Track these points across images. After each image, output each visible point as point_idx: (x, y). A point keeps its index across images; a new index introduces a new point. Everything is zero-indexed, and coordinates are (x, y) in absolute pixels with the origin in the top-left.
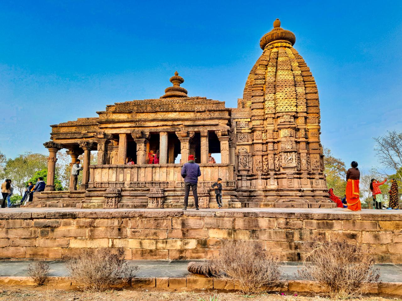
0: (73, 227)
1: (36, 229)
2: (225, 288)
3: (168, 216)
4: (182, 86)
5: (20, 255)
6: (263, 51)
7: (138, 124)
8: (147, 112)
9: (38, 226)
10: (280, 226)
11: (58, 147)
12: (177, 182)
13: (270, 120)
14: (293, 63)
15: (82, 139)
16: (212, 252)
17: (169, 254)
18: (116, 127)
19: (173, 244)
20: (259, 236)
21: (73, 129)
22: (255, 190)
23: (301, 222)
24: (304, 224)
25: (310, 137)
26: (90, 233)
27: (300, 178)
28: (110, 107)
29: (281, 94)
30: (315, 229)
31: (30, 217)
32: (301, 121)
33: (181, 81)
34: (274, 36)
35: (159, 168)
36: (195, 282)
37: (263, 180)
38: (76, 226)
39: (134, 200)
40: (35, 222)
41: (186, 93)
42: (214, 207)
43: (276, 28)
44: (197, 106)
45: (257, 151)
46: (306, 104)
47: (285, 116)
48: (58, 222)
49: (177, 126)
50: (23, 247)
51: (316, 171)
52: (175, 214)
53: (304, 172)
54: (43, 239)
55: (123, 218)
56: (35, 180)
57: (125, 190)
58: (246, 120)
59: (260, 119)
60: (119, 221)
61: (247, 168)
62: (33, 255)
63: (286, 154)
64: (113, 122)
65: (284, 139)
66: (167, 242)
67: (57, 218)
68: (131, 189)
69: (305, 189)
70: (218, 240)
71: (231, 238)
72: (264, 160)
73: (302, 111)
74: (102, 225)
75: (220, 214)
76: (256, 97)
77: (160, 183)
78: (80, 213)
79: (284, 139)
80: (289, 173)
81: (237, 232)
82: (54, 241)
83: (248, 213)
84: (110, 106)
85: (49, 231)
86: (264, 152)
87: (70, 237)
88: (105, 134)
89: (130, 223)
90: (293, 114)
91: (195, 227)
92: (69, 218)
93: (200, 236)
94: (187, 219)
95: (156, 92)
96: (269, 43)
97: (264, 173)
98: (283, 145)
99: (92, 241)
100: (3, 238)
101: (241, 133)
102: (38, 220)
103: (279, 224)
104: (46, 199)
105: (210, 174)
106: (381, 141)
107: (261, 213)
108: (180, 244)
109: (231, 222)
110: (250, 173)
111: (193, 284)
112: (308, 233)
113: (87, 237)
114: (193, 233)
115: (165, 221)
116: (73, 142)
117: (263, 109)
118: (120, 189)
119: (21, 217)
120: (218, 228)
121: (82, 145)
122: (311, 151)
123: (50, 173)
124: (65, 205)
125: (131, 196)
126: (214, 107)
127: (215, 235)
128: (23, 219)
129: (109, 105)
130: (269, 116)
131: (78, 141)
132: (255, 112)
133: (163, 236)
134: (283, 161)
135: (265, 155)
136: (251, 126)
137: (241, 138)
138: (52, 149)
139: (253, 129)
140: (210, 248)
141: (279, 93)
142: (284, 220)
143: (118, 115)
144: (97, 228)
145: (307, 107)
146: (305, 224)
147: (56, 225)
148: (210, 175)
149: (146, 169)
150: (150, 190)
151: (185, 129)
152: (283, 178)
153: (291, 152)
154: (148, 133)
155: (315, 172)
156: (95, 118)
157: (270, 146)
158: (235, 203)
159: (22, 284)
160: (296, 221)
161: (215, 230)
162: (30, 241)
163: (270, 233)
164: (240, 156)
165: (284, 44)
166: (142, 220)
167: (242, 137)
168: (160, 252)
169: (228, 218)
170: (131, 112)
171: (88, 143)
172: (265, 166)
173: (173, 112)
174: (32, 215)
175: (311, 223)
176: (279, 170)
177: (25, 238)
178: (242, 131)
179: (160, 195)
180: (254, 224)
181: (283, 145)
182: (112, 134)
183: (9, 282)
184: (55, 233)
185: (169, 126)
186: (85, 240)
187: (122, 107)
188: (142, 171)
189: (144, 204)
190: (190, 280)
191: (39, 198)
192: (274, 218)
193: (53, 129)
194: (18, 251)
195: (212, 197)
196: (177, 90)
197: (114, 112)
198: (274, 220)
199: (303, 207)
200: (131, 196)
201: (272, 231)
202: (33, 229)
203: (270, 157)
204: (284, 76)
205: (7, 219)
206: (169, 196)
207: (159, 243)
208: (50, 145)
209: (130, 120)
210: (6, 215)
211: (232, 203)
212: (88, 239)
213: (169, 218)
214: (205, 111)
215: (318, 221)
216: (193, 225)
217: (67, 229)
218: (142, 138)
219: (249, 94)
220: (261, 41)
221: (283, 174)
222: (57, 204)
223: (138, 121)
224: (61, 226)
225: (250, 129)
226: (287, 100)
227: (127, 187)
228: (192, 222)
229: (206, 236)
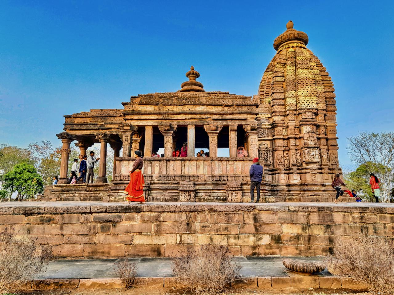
0: (137, 221)
1: (96, 224)
2: (332, 287)
3: (239, 210)
4: (198, 80)
5: (77, 253)
6: (277, 52)
7: (165, 117)
8: (175, 105)
9: (97, 221)
10: (355, 221)
11: (72, 138)
12: (207, 175)
13: (291, 117)
14: (311, 63)
15: (98, 131)
16: (286, 247)
17: (241, 250)
18: (143, 118)
19: (245, 240)
20: (335, 231)
21: (89, 120)
22: (278, 184)
23: (375, 216)
24: (378, 219)
25: (328, 134)
26: (156, 228)
27: (321, 173)
28: (135, 99)
29: (302, 92)
30: (389, 223)
31: (89, 211)
32: (321, 118)
33: (197, 76)
34: (291, 36)
35: (188, 162)
36: (300, 281)
37: (285, 175)
38: (141, 221)
39: (164, 193)
40: (94, 217)
41: (202, 87)
42: (247, 201)
43: (289, 30)
44: (224, 100)
45: (279, 146)
46: (325, 102)
47: (307, 113)
48: (120, 217)
49: (205, 120)
50: (80, 244)
51: (336, 167)
52: (247, 208)
53: (326, 167)
54: (103, 235)
55: (191, 212)
56: (14, 173)
57: (154, 184)
59: (281, 115)
60: (187, 215)
61: (269, 163)
62: (93, 252)
63: (309, 149)
64: (140, 113)
65: (306, 135)
66: (239, 238)
67: (119, 212)
68: (161, 182)
69: (327, 184)
70: (292, 235)
71: (306, 233)
72: (285, 155)
73: (321, 108)
74: (169, 220)
75: (294, 208)
76: (277, 94)
77: (190, 176)
78: (145, 207)
79: (306, 135)
80: (312, 168)
81: (312, 226)
82: (116, 237)
83: (323, 208)
84: (135, 97)
85: (110, 226)
86: (285, 148)
87: (134, 232)
88: (131, 126)
89: (199, 217)
90: (315, 111)
91: (268, 222)
92: (132, 212)
93: (274, 232)
94: (259, 214)
95: (173, 86)
96: (284, 43)
97: (286, 168)
98: (306, 141)
99: (158, 237)
100: (56, 235)
101: (261, 128)
102: (97, 214)
103: (354, 219)
104: (60, 192)
105: (240, 168)
106: (354, 141)
107: (335, 207)
108: (253, 240)
109: (305, 217)
110: (271, 168)
111: (298, 283)
112: (382, 227)
113: (153, 233)
114: (266, 228)
115: (237, 215)
116: (89, 133)
117: (283, 105)
118: (149, 182)
119: (79, 211)
120: (292, 222)
121: (100, 136)
122: (330, 148)
123: (64, 165)
124: (82, 199)
125: (161, 189)
126: (241, 102)
127: (289, 231)
128: (80, 213)
129: (133, 96)
130: (291, 112)
131: (95, 133)
132: (276, 108)
133: (234, 231)
134: (307, 157)
135: (286, 150)
136: (271, 122)
137: (261, 133)
138: (65, 140)
139: (275, 125)
140: (284, 244)
141: (300, 90)
142: (359, 215)
143: (145, 106)
144: (163, 223)
146: (379, 219)
147: (119, 220)
148: (240, 169)
149: (175, 162)
150: (181, 184)
151: (213, 123)
152: (306, 173)
153: (314, 148)
154: (176, 126)
155: (334, 167)
156: (109, 110)
157: (292, 142)
158: (269, 197)
159: (107, 287)
160: (370, 215)
161: (289, 225)
162: (88, 237)
163: (345, 228)
164: (261, 151)
165: (300, 45)
166: (211, 214)
167: (263, 132)
168: (232, 248)
169: (302, 213)
170: (158, 104)
171: (105, 135)
172: (286, 161)
173: (201, 105)
174: (91, 209)
175: (385, 217)
176: (301, 165)
177: (83, 235)
178: (263, 127)
179: (192, 189)
180: (329, 218)
181: (306, 141)
182: (138, 126)
183: (91, 285)
184: (117, 228)
185: (197, 119)
186: (151, 236)
187: (147, 99)
188: (171, 164)
189: (176, 197)
190: (295, 279)
191: (53, 191)
192: (349, 212)
193: (67, 119)
194: (74, 249)
195: (244, 191)
196: (193, 85)
197: (140, 104)
198: (348, 215)
199: (328, 202)
200: (161, 189)
201: (347, 226)
202: (92, 224)
203: (292, 152)
204: (304, 75)
205: (61, 214)
206: (200, 190)
207: (230, 239)
208: (65, 135)
209: (157, 112)
210: (60, 210)
211: (266, 197)
212: (154, 235)
213: (241, 212)
214: (233, 106)
215: (391, 215)
216: (266, 220)
217: (131, 224)
218: (170, 131)
219: (267, 91)
220: (276, 41)
221: (306, 169)
222: (73, 197)
223: (165, 114)
224: (124, 221)
225: (270, 125)
227: (155, 180)
228: (264, 217)
229: (279, 232)
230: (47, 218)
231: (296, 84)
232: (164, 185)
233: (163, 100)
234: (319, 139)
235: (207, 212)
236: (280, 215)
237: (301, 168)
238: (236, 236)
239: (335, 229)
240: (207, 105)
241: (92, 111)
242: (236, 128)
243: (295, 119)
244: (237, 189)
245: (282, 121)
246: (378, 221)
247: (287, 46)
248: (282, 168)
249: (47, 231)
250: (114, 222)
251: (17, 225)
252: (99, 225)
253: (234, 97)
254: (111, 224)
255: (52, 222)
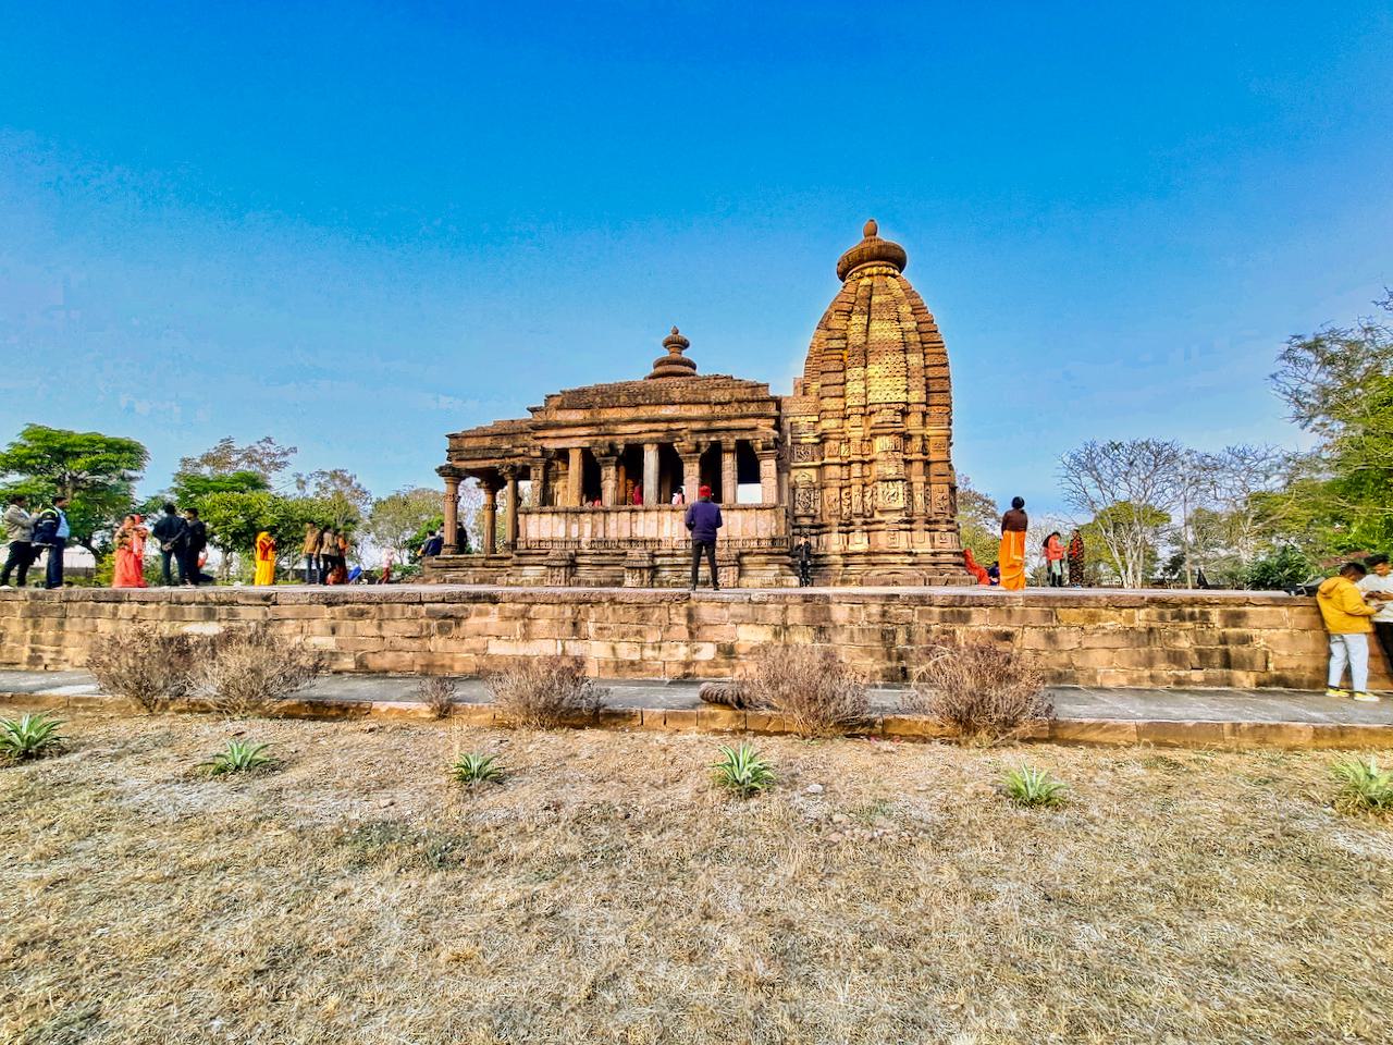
0: (492, 618)
1: (431, 621)
4: (686, 354)
6: (843, 284)
13: (855, 420)
27: (911, 530)
32: (914, 422)
33: (684, 345)
36: (713, 717)
41: (694, 367)
43: (869, 238)
47: (884, 411)
48: (466, 610)
58: (810, 419)
61: (812, 512)
62: (427, 666)
63: (886, 484)
64: (559, 426)
65: (881, 457)
66: (660, 648)
68: (594, 551)
69: (919, 551)
70: (755, 644)
73: (917, 400)
77: (646, 541)
81: (791, 629)
83: (813, 596)
88: (544, 450)
89: (594, 613)
96: (867, 261)
98: (880, 468)
101: (799, 444)
102: (431, 605)
103: (869, 615)
106: (1067, 459)
107: (835, 595)
110: (817, 521)
113: (518, 637)
114: (708, 633)
115: (657, 610)
117: (841, 397)
118: (573, 552)
119: (403, 600)
120: (755, 622)
124: (477, 580)
125: (594, 565)
133: (653, 636)
136: (819, 431)
140: (739, 659)
142: (879, 608)
143: (567, 412)
145: (927, 393)
153: (896, 480)
154: (622, 447)
155: (939, 518)
157: (856, 469)
163: (852, 633)
165: (885, 270)
171: (514, 468)
172: (845, 508)
176: (872, 516)
178: (803, 441)
181: (880, 468)
185: (662, 431)
189: (618, 579)
197: (559, 408)
200: (594, 565)
201: (856, 627)
209: (588, 422)
213: (664, 604)
214: (729, 403)
221: (880, 522)
224: (472, 617)
226: (888, 379)
230: (358, 609)
231: (865, 355)
232: (600, 558)
233: (602, 398)
234: (908, 462)
235: (607, 604)
236: (734, 609)
237: (870, 524)
238: (656, 645)
239: (832, 634)
240: (681, 404)
241: (496, 424)
242: (732, 447)
243: (864, 424)
244: (728, 563)
245: (838, 428)
246: (916, 620)
247: (859, 274)
248: (834, 521)
249: (359, 631)
250: (456, 618)
251: (316, 621)
252: (435, 623)
253: (740, 384)
254: (453, 622)
255: (365, 616)
